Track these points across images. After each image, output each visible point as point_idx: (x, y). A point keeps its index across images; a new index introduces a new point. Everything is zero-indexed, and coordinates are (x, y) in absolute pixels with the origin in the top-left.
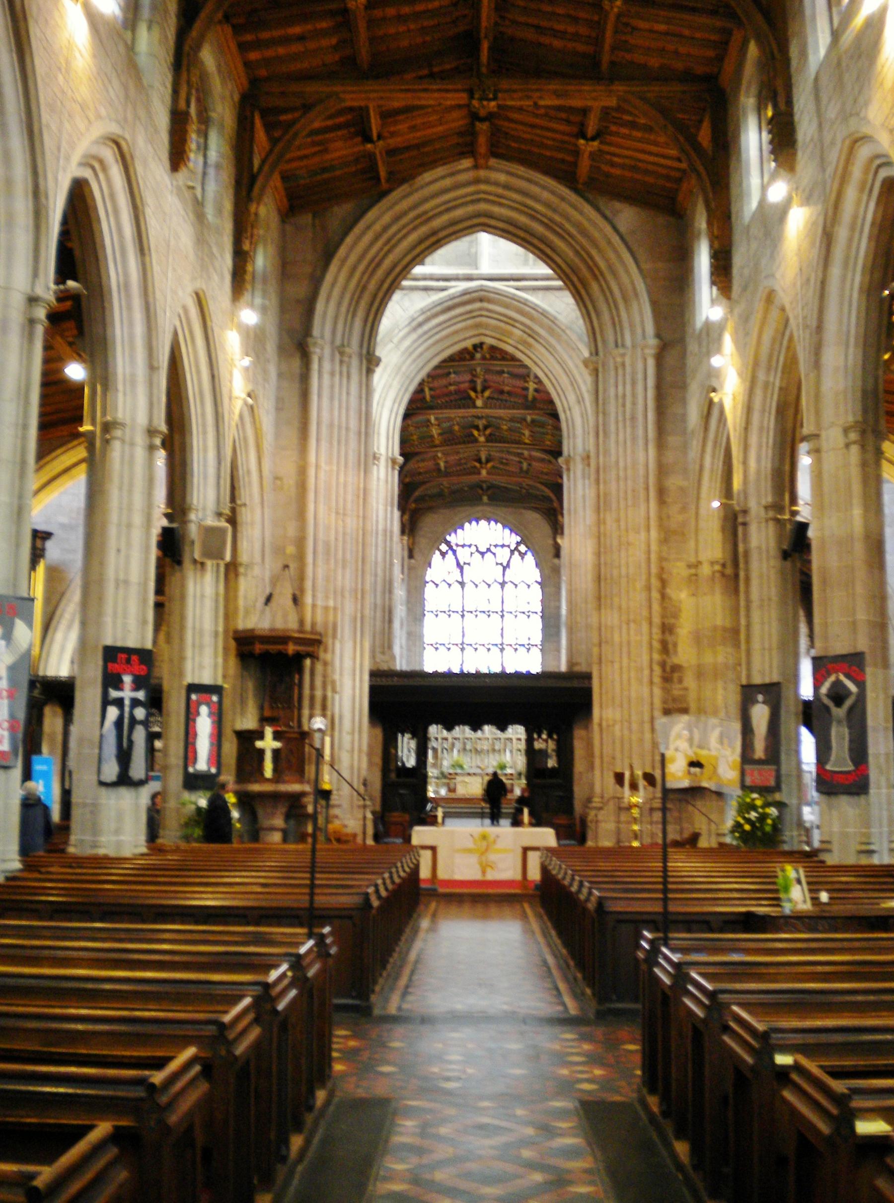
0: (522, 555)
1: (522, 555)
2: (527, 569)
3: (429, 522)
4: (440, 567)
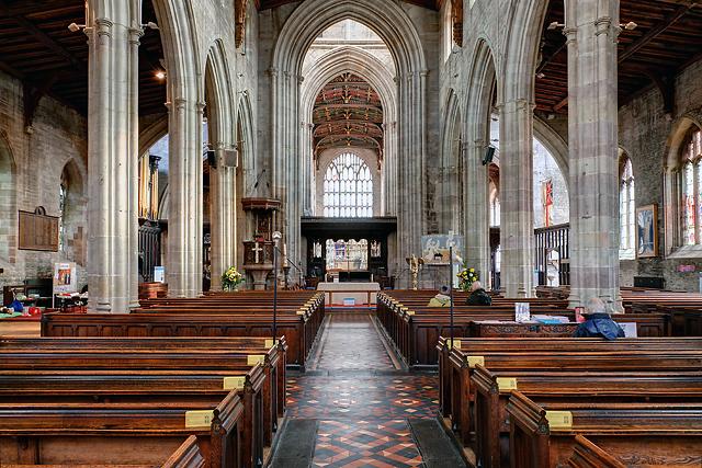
0: (365, 169)
1: (365, 169)
2: (366, 174)
3: (325, 155)
4: (330, 174)
